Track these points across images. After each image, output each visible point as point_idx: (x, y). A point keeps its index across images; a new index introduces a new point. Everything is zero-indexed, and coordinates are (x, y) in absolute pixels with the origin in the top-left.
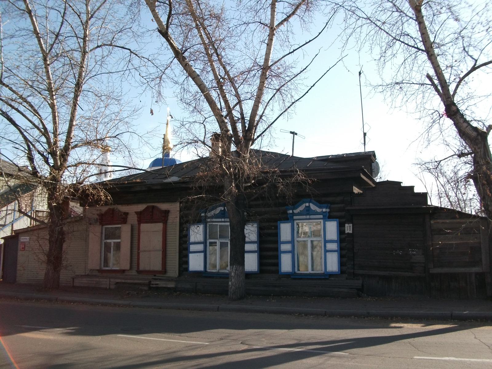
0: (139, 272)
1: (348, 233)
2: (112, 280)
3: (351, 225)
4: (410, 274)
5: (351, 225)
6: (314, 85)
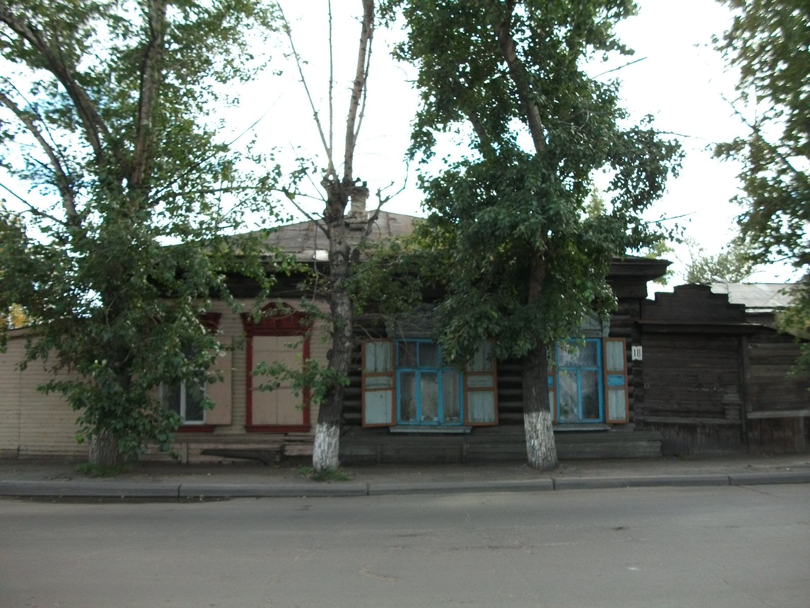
0: (250, 428)
1: (636, 361)
2: (192, 446)
3: (640, 348)
4: (718, 421)
5: (640, 348)
6: (318, 121)
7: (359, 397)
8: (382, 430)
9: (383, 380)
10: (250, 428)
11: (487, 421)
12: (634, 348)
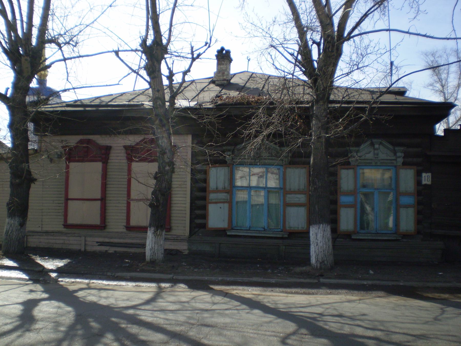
0: (129, 228)
2: (88, 239)
3: (430, 174)
5: (430, 174)
7: (204, 208)
8: (221, 232)
9: (223, 196)
10: (129, 228)
11: (300, 229)
12: (424, 175)
